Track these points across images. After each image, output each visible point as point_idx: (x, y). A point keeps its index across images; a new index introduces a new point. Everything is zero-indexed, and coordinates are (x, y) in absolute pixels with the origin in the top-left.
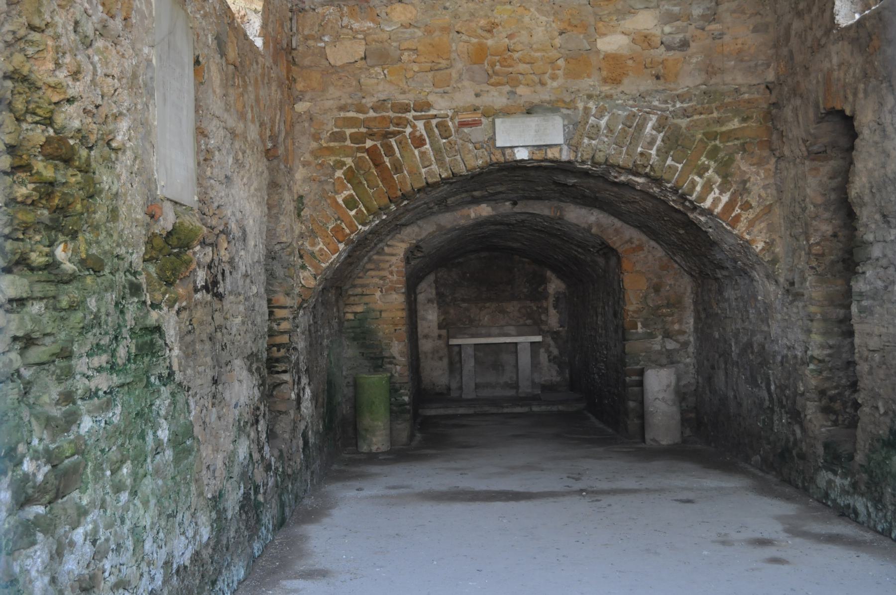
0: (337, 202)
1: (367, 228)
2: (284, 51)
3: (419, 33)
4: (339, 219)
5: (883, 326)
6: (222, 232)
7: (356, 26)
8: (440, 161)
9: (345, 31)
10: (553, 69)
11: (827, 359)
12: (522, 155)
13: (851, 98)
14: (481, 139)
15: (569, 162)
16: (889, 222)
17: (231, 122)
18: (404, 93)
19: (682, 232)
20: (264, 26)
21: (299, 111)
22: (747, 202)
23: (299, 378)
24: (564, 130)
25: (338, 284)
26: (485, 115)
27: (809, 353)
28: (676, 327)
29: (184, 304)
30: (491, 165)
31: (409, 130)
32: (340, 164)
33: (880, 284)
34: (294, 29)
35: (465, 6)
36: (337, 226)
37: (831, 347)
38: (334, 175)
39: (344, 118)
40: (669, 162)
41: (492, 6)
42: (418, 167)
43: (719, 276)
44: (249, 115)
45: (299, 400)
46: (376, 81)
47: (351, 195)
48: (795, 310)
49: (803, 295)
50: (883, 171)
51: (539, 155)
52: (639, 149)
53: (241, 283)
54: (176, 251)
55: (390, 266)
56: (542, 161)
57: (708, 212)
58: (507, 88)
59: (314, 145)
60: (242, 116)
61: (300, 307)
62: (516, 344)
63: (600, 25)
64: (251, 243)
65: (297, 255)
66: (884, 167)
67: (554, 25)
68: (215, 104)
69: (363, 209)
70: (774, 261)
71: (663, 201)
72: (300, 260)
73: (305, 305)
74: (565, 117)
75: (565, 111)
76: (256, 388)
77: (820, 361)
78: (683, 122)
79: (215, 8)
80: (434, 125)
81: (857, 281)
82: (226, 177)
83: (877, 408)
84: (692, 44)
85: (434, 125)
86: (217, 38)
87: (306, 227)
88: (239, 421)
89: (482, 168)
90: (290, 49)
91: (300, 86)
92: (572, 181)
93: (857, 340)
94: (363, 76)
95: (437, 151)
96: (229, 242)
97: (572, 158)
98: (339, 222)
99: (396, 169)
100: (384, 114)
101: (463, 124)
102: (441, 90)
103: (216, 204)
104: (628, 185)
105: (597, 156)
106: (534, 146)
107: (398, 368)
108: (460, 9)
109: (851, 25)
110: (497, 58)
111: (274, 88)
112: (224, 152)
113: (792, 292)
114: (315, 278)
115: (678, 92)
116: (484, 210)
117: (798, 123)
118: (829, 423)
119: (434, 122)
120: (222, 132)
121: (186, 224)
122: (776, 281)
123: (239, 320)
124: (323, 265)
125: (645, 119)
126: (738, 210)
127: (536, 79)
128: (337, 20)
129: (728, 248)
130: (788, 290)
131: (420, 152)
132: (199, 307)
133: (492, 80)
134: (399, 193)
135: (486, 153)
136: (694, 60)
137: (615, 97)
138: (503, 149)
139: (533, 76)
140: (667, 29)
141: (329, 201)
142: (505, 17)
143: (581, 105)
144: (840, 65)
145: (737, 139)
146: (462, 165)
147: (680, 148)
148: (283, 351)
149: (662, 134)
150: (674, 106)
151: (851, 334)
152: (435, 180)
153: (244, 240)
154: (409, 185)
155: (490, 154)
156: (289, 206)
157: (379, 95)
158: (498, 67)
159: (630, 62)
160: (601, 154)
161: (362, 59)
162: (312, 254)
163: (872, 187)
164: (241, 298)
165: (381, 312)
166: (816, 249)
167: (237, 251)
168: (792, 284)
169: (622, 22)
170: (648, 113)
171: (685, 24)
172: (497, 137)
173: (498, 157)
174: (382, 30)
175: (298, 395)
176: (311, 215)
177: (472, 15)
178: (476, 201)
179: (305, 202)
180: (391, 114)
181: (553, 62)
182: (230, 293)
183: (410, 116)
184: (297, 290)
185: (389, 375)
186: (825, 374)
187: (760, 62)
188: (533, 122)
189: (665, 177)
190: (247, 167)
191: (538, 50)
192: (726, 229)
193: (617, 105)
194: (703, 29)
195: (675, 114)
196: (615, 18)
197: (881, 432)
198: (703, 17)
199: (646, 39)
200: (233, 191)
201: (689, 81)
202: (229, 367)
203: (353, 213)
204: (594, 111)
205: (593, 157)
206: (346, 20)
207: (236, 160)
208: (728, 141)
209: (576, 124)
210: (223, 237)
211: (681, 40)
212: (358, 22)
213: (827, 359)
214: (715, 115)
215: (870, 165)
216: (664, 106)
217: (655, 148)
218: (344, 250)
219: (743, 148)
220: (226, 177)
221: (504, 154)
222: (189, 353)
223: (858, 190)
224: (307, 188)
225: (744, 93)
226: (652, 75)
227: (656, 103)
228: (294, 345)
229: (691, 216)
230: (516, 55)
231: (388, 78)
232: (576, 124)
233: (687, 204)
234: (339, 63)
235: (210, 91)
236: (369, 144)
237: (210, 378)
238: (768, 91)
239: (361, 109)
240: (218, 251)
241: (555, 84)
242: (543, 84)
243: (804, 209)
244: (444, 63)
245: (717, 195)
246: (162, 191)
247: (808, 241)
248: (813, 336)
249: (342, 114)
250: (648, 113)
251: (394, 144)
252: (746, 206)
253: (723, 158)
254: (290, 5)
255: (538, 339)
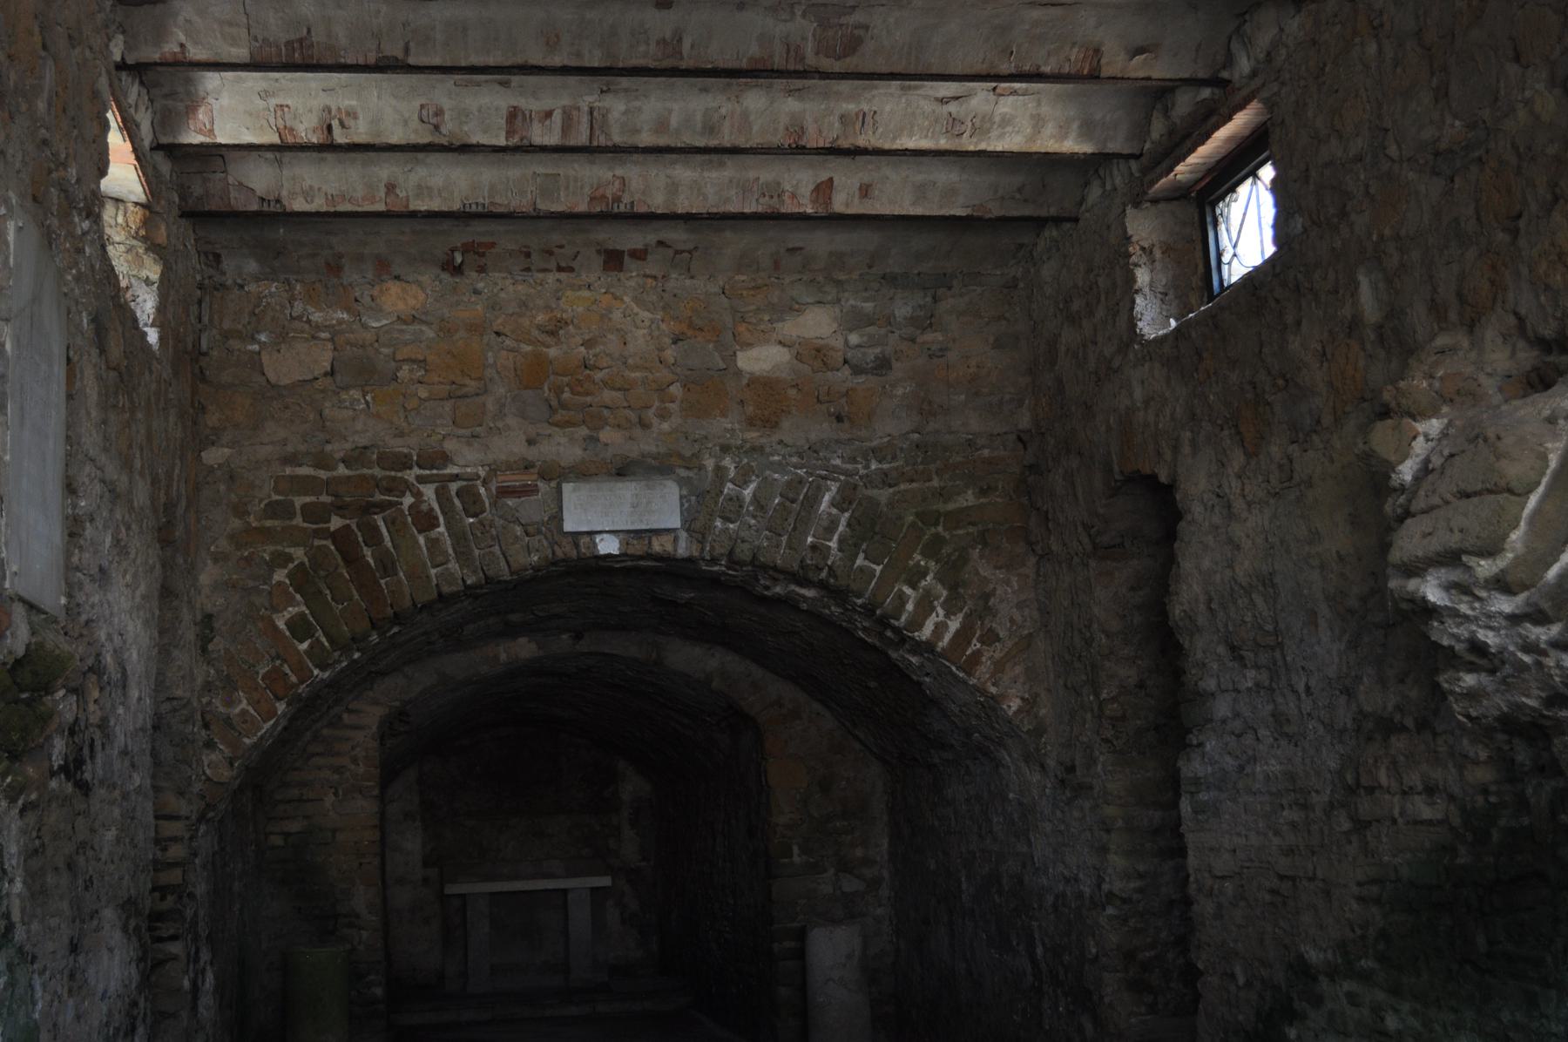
0: (275, 628)
1: (326, 675)
2: (186, 353)
3: (430, 333)
4: (278, 657)
5: (1239, 834)
6: (91, 669)
7: (317, 317)
8: (463, 556)
9: (297, 324)
10: (663, 401)
11: (1135, 896)
12: (608, 546)
13: (1168, 455)
14: (537, 518)
15: (690, 560)
16: (1242, 658)
17: (112, 472)
18: (401, 435)
19: (873, 684)
20: (161, 309)
21: (211, 462)
22: (991, 630)
23: (197, 952)
24: (682, 505)
25: (264, 779)
26: (543, 476)
27: (1106, 887)
28: (859, 852)
29: (33, 797)
30: (554, 564)
31: (408, 500)
32: (282, 559)
33: (1230, 763)
34: (206, 319)
35: (511, 288)
36: (276, 670)
37: (1141, 876)
38: (271, 578)
39: (291, 477)
40: (860, 561)
41: (557, 291)
42: (424, 564)
43: (937, 760)
44: (138, 464)
45: (195, 988)
46: (351, 413)
47: (302, 615)
48: (1076, 814)
49: (1091, 788)
50: (1228, 573)
51: (637, 548)
52: (810, 539)
53: (117, 765)
54: (24, 696)
55: (353, 748)
56: (641, 558)
57: (927, 648)
58: (584, 431)
59: (236, 523)
60: (126, 464)
61: (202, 818)
62: (565, 891)
63: (742, 328)
64: (134, 693)
65: (199, 723)
66: (1231, 567)
67: (663, 326)
68: (91, 440)
69: (324, 639)
70: (1039, 731)
71: (847, 630)
72: (203, 732)
73: (211, 814)
74: (682, 482)
75: (683, 473)
76: (134, 965)
77: (1124, 901)
78: (883, 495)
79: (92, 266)
80: (453, 493)
81: (1189, 760)
82: (101, 569)
83: (1233, 976)
84: (896, 365)
85: (453, 493)
86: (95, 320)
87: (217, 671)
88: (107, 1024)
89: (536, 569)
90: (198, 354)
91: (212, 419)
92: (687, 595)
93: (1192, 861)
94: (327, 404)
95: (459, 537)
96: (102, 689)
97: (696, 554)
98: (278, 662)
99: (385, 568)
100: (365, 471)
101: (505, 492)
102: (467, 432)
103: (84, 617)
104: (788, 602)
105: (738, 550)
106: (629, 532)
107: (365, 934)
108: (503, 295)
109: (1165, 336)
110: (566, 379)
111: (172, 419)
112: (99, 523)
113: (1071, 783)
114: (231, 764)
115: (875, 443)
116: (524, 648)
117: (1075, 495)
118: (1143, 1010)
119: (454, 487)
120: (98, 488)
121: (49, 646)
122: (1042, 766)
123: (111, 835)
124: (247, 741)
125: (819, 488)
126: (976, 645)
127: (633, 416)
128: (283, 307)
129: (957, 710)
130: (1062, 781)
131: (427, 539)
132: (54, 805)
133: (558, 417)
134: (390, 611)
135: (545, 543)
136: (900, 391)
137: (768, 450)
138: (576, 535)
139: (627, 411)
140: (854, 339)
141: (260, 625)
142: (580, 309)
143: (710, 463)
144: (1147, 403)
145: (973, 524)
146: (503, 563)
147: (877, 538)
148: (170, 899)
149: (847, 515)
150: (867, 467)
151: (1182, 852)
152: (454, 589)
153: (124, 687)
154: (408, 597)
155: (553, 543)
156: (189, 633)
157: (356, 438)
158: (566, 395)
159: (792, 392)
160: (746, 546)
161: (326, 374)
162: (228, 721)
163: (1210, 600)
164: (117, 792)
165: (334, 831)
166: (1112, 709)
167: (114, 707)
168: (1071, 769)
169: (779, 325)
170: (825, 478)
171: (883, 331)
172: (566, 515)
173: (566, 550)
174: (365, 326)
175: (194, 984)
176: (227, 650)
177: (523, 304)
178: (511, 632)
179: (216, 625)
180: (377, 472)
181: (662, 390)
182: (102, 782)
183: (410, 475)
184: (197, 787)
185: (348, 946)
186: (1132, 923)
187: (1007, 397)
188: (627, 490)
189: (854, 587)
190: (132, 556)
191: (636, 368)
192: (955, 676)
193: (772, 463)
194: (913, 340)
195: (868, 481)
196: (767, 318)
197: (1241, 1017)
198: (912, 320)
199: (815, 354)
200: (110, 597)
201: (891, 426)
202: (95, 922)
203: (304, 646)
204: (732, 475)
205: (731, 552)
206: (298, 307)
207: (117, 541)
208: (957, 528)
209: (701, 495)
210: (94, 678)
211: (877, 358)
212: (321, 310)
213: (1135, 896)
214: (935, 483)
215: (1206, 563)
216: (849, 466)
217: (836, 537)
218: (284, 714)
219: (983, 539)
220: (101, 569)
221: (577, 545)
222: (37, 892)
223: (1186, 607)
224: (221, 601)
225: (983, 447)
226: (830, 415)
227: (838, 462)
228: (190, 889)
229: (894, 655)
230: (599, 375)
231: (373, 409)
232: (701, 495)
233: (889, 633)
234: (285, 381)
235: (83, 412)
236: (336, 523)
237: (66, 941)
238: (1020, 446)
239: (322, 462)
240: (86, 703)
241: (666, 426)
242: (645, 425)
243: (1088, 642)
244: (472, 385)
245: (941, 618)
246: (12, 583)
247: (1097, 695)
248: (1112, 857)
249: (288, 471)
250: (825, 478)
251: (381, 524)
252: (990, 638)
253: (949, 555)
254: (198, 277)
255: (606, 881)
